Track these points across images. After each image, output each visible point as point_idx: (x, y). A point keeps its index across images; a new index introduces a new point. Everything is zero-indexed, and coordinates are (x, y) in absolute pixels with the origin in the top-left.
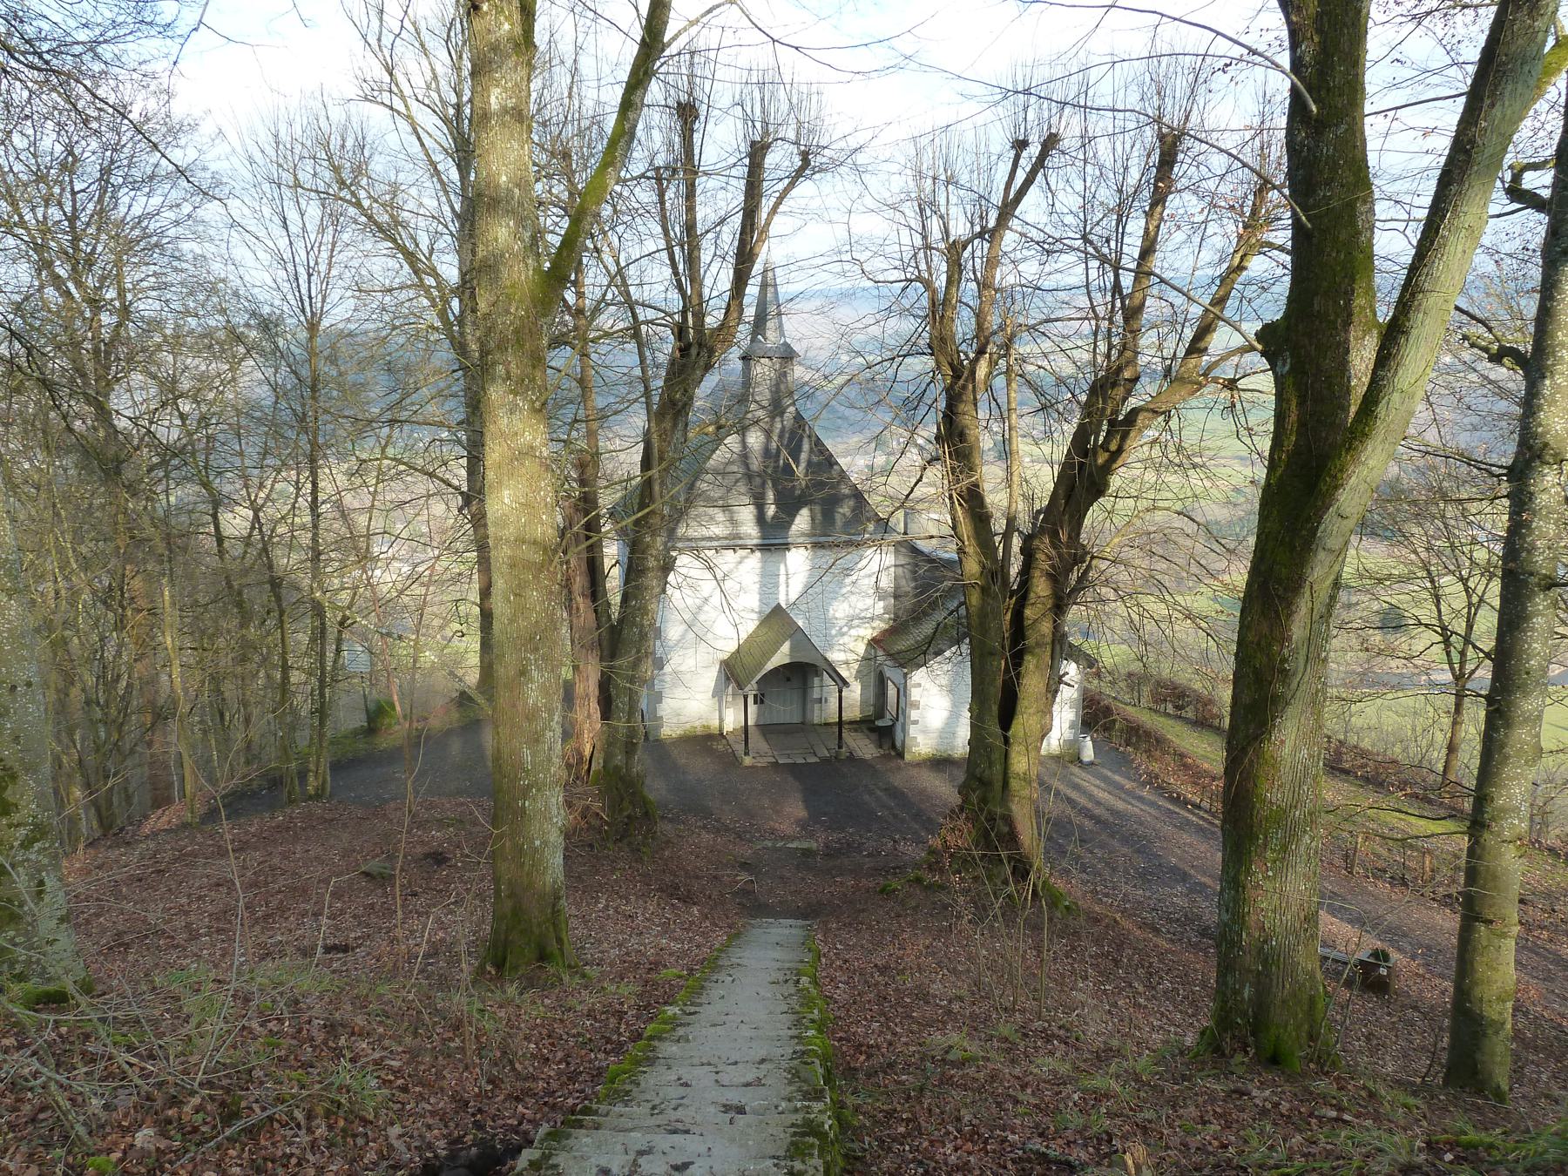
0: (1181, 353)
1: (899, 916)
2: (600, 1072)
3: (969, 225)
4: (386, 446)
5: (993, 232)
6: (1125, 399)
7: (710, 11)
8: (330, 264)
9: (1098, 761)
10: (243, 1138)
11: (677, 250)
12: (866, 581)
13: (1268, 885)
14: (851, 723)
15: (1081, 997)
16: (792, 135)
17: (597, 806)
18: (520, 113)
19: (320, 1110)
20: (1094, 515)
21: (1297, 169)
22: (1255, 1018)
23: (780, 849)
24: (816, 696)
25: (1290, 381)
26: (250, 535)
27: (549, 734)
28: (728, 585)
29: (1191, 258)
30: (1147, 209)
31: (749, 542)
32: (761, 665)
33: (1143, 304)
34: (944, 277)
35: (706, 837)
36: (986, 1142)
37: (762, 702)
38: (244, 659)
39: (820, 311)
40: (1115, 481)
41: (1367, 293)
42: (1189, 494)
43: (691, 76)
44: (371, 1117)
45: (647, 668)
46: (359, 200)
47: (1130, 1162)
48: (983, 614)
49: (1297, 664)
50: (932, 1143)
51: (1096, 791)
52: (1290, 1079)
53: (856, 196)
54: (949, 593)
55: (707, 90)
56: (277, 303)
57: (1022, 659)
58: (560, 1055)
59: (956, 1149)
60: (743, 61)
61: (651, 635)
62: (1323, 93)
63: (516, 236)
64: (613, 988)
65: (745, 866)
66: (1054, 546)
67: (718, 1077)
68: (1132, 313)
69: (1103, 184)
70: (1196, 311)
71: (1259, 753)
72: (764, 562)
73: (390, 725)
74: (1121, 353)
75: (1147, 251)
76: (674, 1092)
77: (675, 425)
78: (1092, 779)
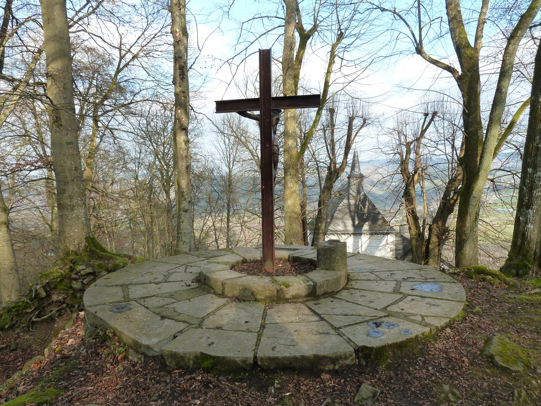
11: (329, 146)
49: (468, 232)
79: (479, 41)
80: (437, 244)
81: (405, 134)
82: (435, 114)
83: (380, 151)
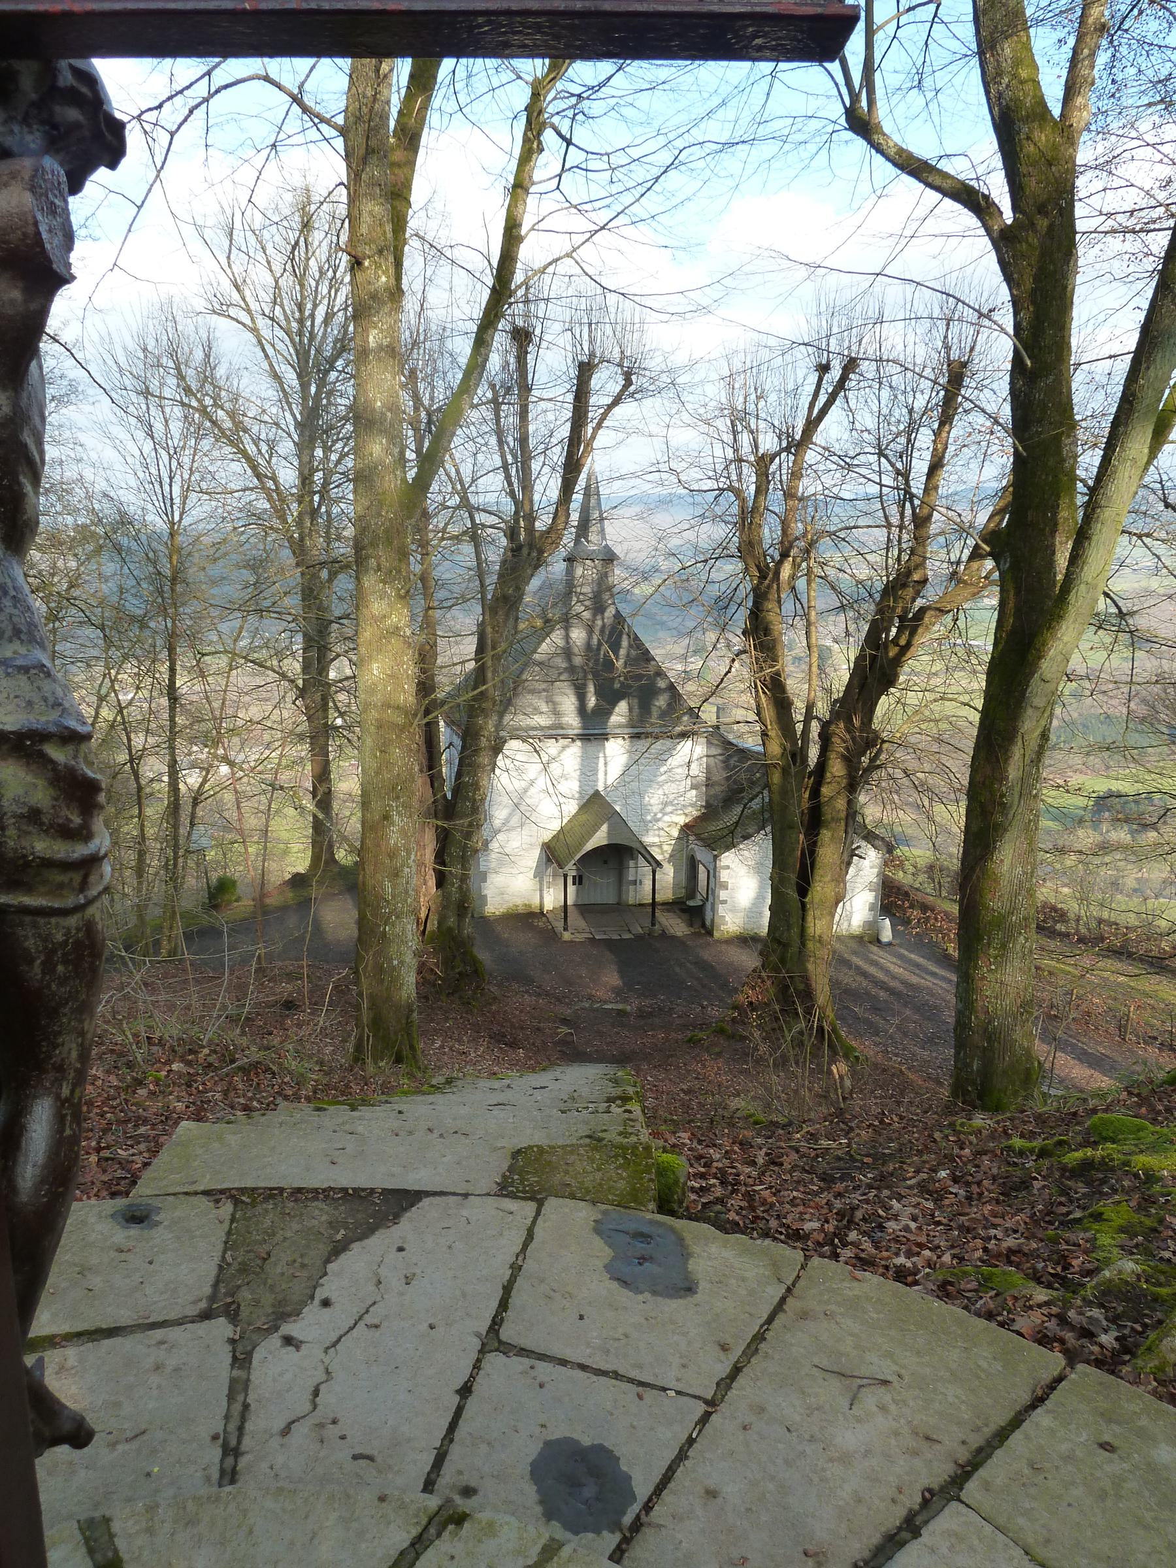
0: (965, 557)
3: (776, 439)
6: (914, 600)
9: (894, 942)
13: (990, 977)
14: (664, 904)
18: (393, 349)
20: (884, 704)
23: (597, 1010)
24: (631, 878)
27: (407, 870)
30: (936, 426)
31: (570, 732)
34: (753, 488)
37: (580, 883)
39: (640, 517)
41: (1069, 507)
48: (785, 792)
49: (1012, 798)
51: (892, 967)
53: (674, 411)
63: (387, 451)
65: (565, 1021)
66: (848, 731)
68: (921, 522)
71: (984, 871)
79: (1079, 100)
80: (844, 782)
82: (851, 365)
83: (674, 479)
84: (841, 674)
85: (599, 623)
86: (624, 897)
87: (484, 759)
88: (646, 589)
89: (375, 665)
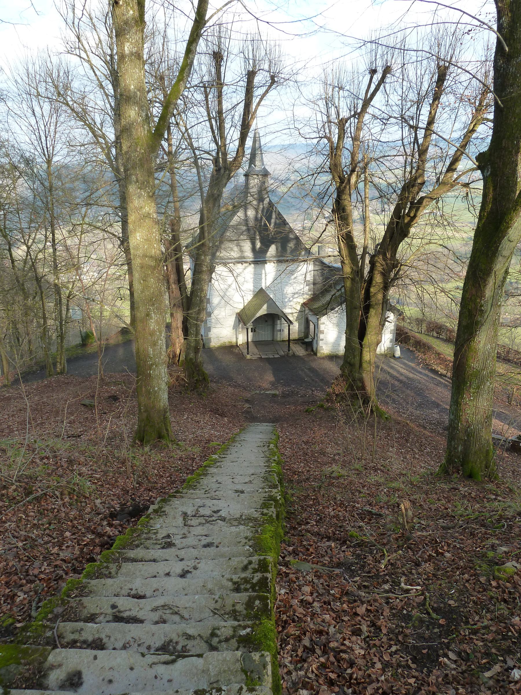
0: (445, 169)
1: (313, 421)
2: (184, 481)
4: (85, 216)
5: (359, 114)
6: (418, 193)
7: (226, 4)
8: (55, 132)
10: (34, 502)
12: (300, 278)
13: (471, 403)
14: (294, 340)
15: (390, 454)
16: (266, 67)
17: (182, 375)
18: (139, 55)
19: (66, 492)
20: (402, 246)
21: (498, 78)
22: (463, 459)
24: (278, 328)
25: (490, 180)
26: (26, 259)
27: (160, 342)
28: (239, 279)
29: (451, 126)
30: (431, 102)
31: (248, 260)
32: (254, 314)
33: (427, 149)
34: (337, 136)
35: (231, 389)
36: (346, 507)
37: (255, 331)
38: (26, 314)
40: (412, 230)
42: (446, 237)
43: (220, 37)
44: (88, 496)
45: (203, 315)
46: (67, 102)
47: (403, 508)
48: (352, 291)
49: (487, 307)
50: (324, 508)
51: (401, 369)
52: (477, 484)
53: (296, 97)
54: (336, 283)
55: (227, 45)
56: (33, 151)
57: (369, 310)
58: (167, 475)
59: (334, 510)
60: (244, 31)
61: (205, 301)
62: (512, 42)
64: (190, 449)
65: (247, 401)
67: (233, 480)
68: (423, 152)
69: (411, 91)
70: (452, 151)
71: (469, 347)
72: (255, 268)
73: (92, 343)
74: (417, 171)
75: (431, 122)
76: (215, 486)
77: (214, 205)
78: (399, 364)
80: (382, 286)
81: (337, 104)
84: (381, 232)
85: (261, 206)
86: (275, 337)
87: (205, 277)
88: (283, 189)
89: (138, 234)
